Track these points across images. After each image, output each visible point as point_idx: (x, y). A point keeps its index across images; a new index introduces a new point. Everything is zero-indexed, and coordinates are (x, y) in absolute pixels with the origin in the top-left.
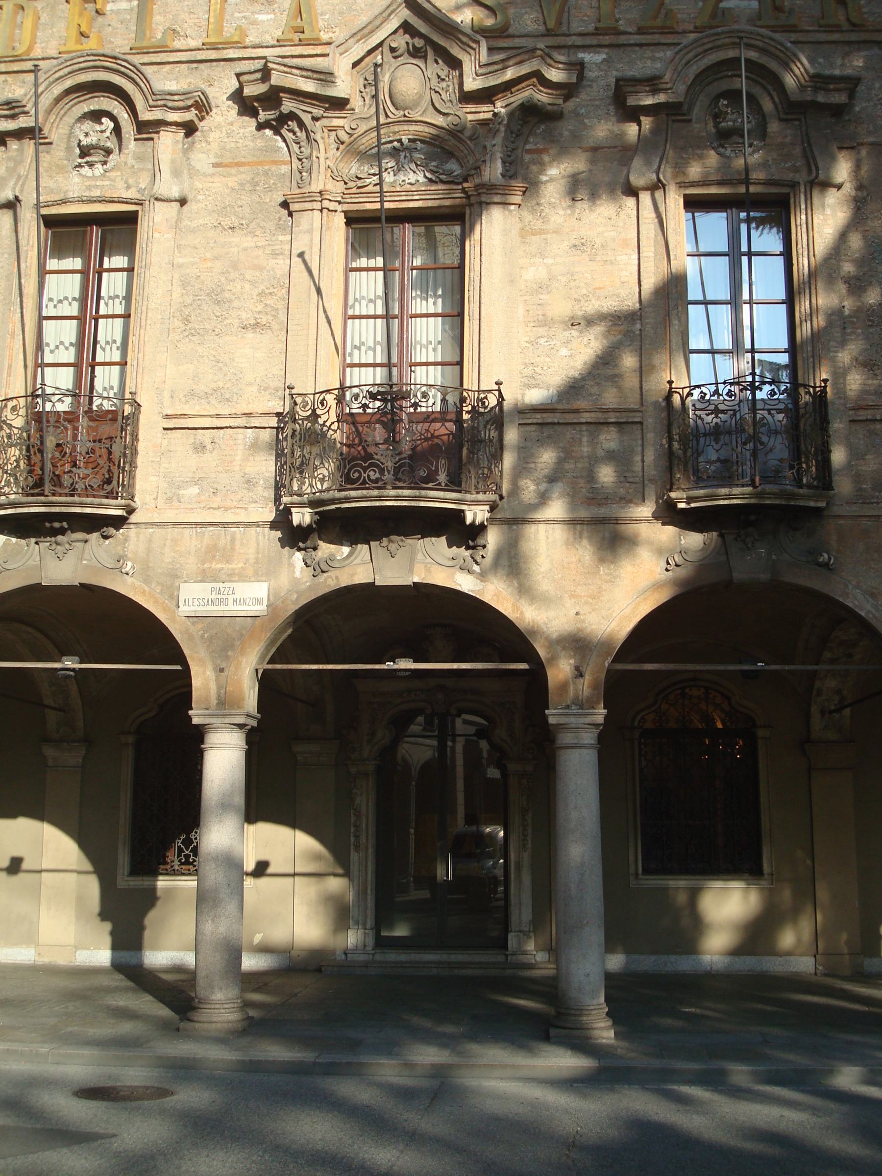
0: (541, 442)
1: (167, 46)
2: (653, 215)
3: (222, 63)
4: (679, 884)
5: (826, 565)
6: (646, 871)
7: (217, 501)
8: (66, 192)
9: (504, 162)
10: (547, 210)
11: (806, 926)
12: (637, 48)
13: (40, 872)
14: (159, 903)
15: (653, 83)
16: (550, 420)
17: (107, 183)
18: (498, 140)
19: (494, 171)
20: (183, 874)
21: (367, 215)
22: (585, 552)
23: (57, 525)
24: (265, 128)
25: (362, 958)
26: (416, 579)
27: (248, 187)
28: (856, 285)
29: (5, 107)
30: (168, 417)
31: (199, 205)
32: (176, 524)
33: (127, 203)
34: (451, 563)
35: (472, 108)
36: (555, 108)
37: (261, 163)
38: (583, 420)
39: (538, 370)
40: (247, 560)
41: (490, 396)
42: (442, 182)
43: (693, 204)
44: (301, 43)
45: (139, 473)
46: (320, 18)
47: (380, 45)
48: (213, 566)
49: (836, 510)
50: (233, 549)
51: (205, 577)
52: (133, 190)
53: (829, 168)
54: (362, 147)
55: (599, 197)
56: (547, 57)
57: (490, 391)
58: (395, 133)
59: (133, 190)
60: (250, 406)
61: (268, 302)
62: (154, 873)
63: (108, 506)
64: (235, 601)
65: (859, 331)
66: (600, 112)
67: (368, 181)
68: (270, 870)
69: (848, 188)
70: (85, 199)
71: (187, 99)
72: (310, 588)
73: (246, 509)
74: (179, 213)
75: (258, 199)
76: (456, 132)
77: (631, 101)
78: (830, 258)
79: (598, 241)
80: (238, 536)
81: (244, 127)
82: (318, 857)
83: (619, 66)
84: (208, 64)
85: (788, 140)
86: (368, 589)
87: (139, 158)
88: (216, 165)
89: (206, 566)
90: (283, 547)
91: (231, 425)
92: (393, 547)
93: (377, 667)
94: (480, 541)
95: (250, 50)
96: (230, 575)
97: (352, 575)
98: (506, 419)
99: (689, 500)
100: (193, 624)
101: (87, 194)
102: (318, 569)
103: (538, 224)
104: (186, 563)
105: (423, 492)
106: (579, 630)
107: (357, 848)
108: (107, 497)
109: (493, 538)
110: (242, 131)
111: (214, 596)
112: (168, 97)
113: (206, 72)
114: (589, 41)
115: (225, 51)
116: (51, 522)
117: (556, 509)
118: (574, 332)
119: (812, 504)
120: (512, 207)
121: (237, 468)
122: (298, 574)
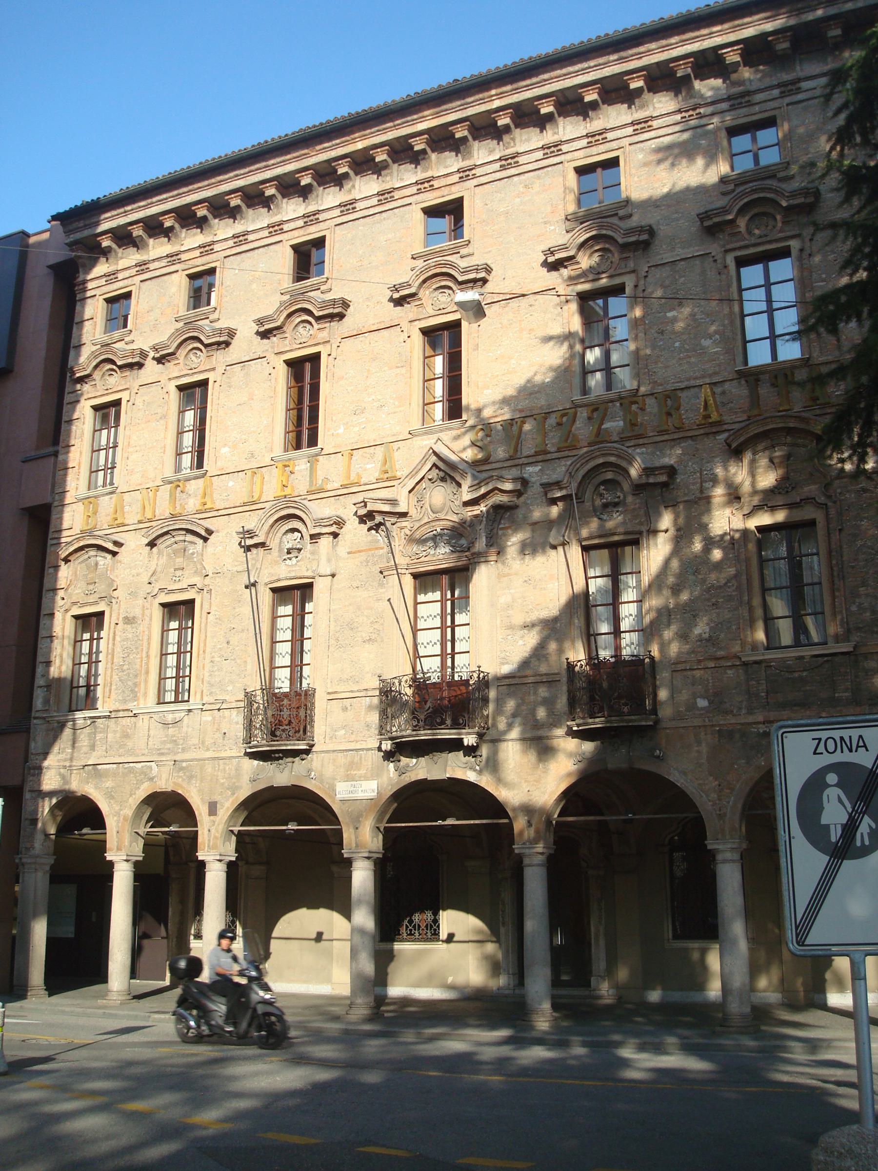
0: (510, 695)
1: (323, 489)
2: (564, 560)
4: (695, 945)
5: (658, 757)
6: (676, 937)
7: (353, 737)
9: (487, 538)
10: (511, 562)
11: (775, 973)
12: (557, 461)
13: (332, 940)
14: (395, 959)
15: (558, 485)
16: (513, 683)
18: (483, 526)
19: (480, 544)
20: (409, 941)
22: (532, 756)
23: (277, 755)
25: (507, 992)
26: (448, 776)
28: (676, 590)
30: (329, 693)
32: (334, 751)
34: (464, 766)
35: (469, 508)
36: (512, 503)
37: (370, 550)
38: (530, 681)
39: (508, 654)
41: (474, 674)
43: (585, 549)
44: (388, 479)
45: (316, 725)
46: (396, 463)
47: (423, 478)
48: (352, 772)
49: (663, 725)
50: (361, 763)
51: (349, 778)
52: (310, 571)
53: (657, 521)
54: (417, 536)
55: (538, 552)
56: (500, 478)
57: (474, 672)
58: (433, 526)
59: (310, 571)
62: (393, 940)
63: (298, 745)
65: (679, 616)
66: (538, 501)
67: (421, 555)
68: (455, 939)
69: (672, 531)
72: (397, 783)
74: (332, 581)
76: (463, 523)
77: (550, 496)
78: (660, 575)
80: (363, 756)
82: (480, 932)
83: (548, 472)
85: (637, 506)
87: (313, 553)
88: (349, 553)
92: (435, 758)
93: (434, 824)
94: (478, 753)
96: (360, 777)
98: (490, 684)
99: (578, 725)
100: (344, 804)
102: (401, 772)
103: (506, 571)
105: (438, 731)
106: (530, 800)
107: (504, 924)
108: (298, 740)
109: (484, 751)
114: (531, 460)
116: (274, 754)
117: (515, 733)
118: (526, 631)
119: (644, 723)
120: (492, 563)
121: (362, 719)
122: (392, 775)
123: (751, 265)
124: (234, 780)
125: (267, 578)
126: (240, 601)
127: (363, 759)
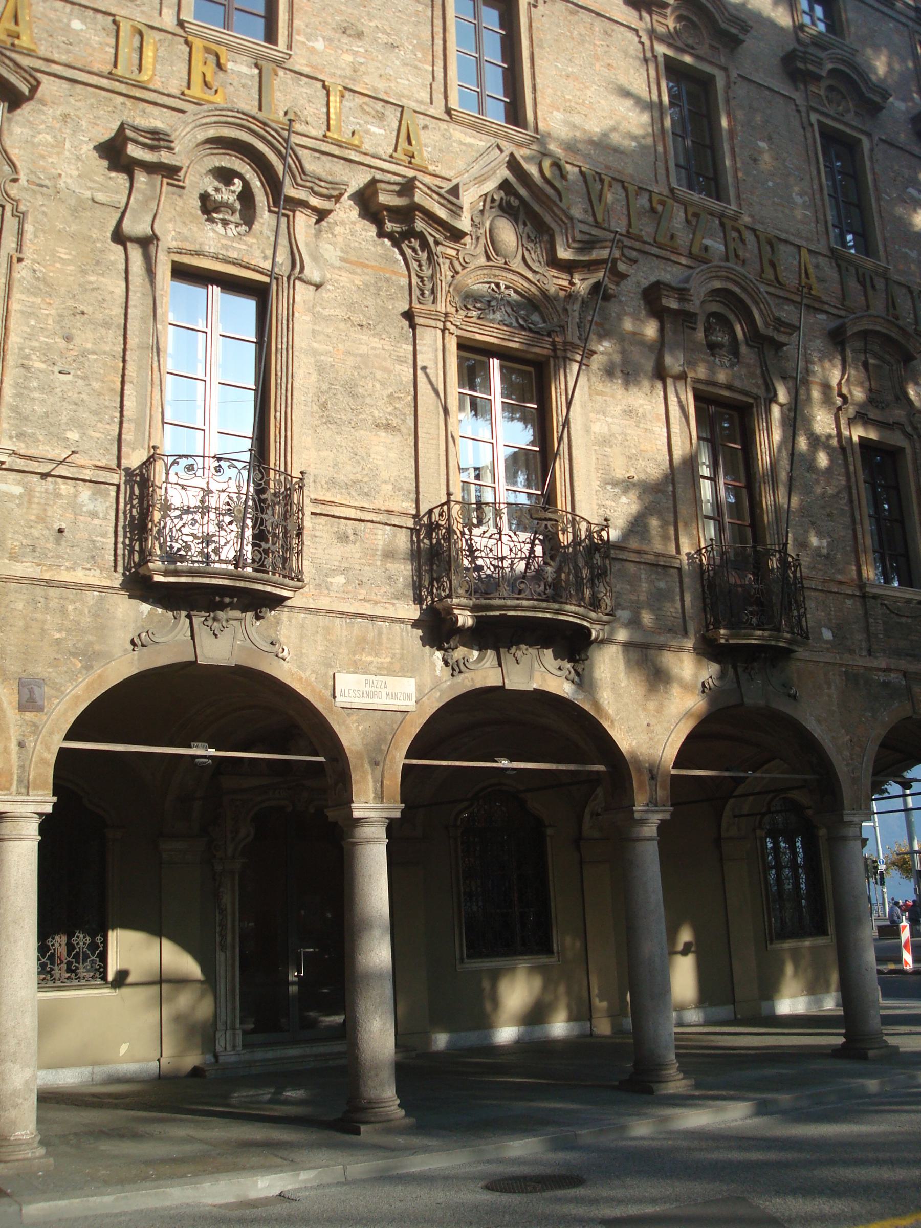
3: (342, 161)
7: (362, 593)
8: (201, 244)
17: (244, 247)
21: (478, 345)
24: (385, 237)
26: (535, 686)
27: (372, 289)
29: (149, 135)
31: (329, 294)
32: (329, 612)
33: (254, 270)
40: (394, 655)
42: (530, 330)
50: (380, 643)
58: (495, 276)
60: (386, 503)
61: (397, 406)
64: (388, 695)
68: (130, 979)
70: (220, 257)
71: (332, 189)
72: (451, 687)
73: (393, 604)
75: (381, 303)
79: (641, 411)
80: (385, 631)
81: (366, 230)
83: (645, 269)
84: (330, 158)
86: (499, 690)
89: (357, 657)
90: (424, 645)
91: (374, 519)
95: (369, 158)
97: (485, 678)
101: (223, 252)
104: (338, 653)
107: (223, 948)
110: (364, 233)
111: (368, 689)
112: (317, 181)
113: (328, 165)
115: (347, 151)
116: (222, 596)
123: (504, 79)
124: (89, 638)
125: (174, 239)
126: (98, 263)
127: (384, 637)
